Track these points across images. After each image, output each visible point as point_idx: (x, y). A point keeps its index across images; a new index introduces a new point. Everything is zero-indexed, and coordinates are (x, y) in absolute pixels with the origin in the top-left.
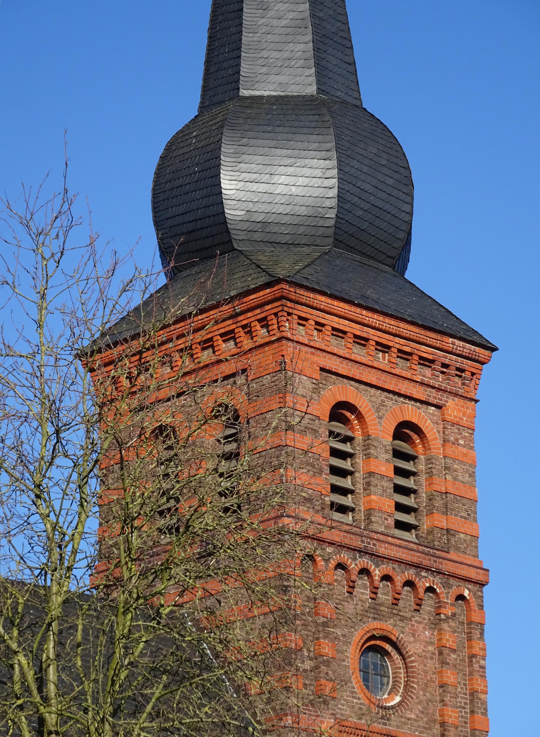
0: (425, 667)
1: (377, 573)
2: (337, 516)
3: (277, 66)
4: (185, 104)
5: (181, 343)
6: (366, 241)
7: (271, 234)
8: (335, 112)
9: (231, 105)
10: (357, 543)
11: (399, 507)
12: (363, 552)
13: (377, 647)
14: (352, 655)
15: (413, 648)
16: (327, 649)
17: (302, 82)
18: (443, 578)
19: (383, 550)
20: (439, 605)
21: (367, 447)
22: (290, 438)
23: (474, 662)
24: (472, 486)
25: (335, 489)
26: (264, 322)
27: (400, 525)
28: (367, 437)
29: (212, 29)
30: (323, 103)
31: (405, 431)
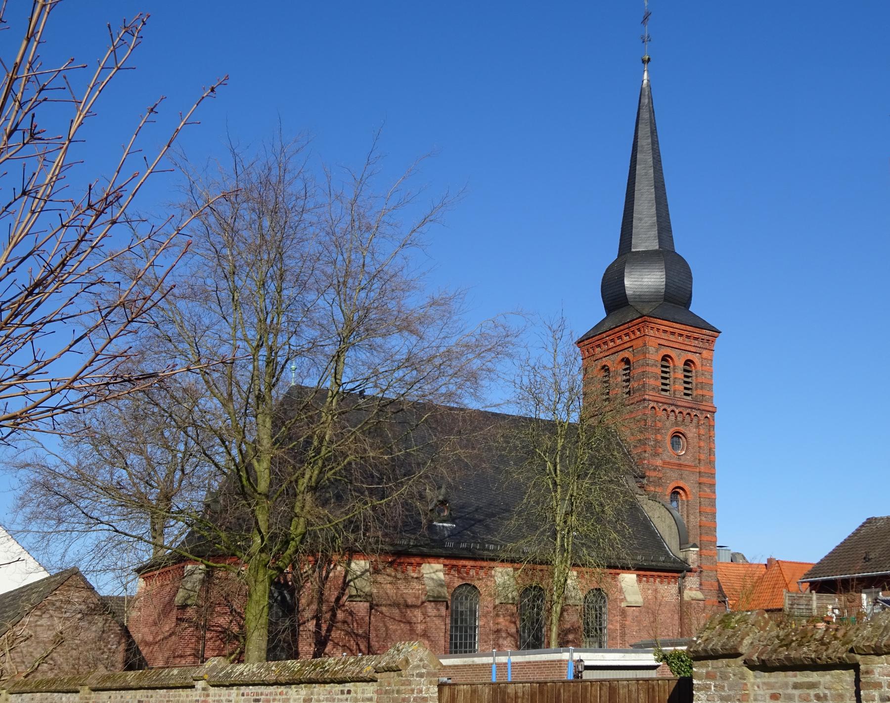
0: (693, 441)
1: (677, 411)
2: (663, 393)
3: (645, 240)
4: (614, 256)
5: (611, 338)
6: (676, 299)
7: (642, 299)
8: (665, 254)
9: (628, 255)
10: (670, 402)
11: (686, 388)
12: (672, 405)
13: (677, 435)
14: (668, 439)
15: (689, 435)
16: (659, 437)
17: (654, 245)
18: (700, 411)
19: (679, 403)
20: (699, 420)
21: (674, 369)
22: (648, 369)
23: (710, 439)
24: (711, 379)
25: (663, 384)
26: (639, 330)
27: (686, 394)
28: (674, 366)
29: (622, 228)
30: (661, 252)
31: (688, 362)
